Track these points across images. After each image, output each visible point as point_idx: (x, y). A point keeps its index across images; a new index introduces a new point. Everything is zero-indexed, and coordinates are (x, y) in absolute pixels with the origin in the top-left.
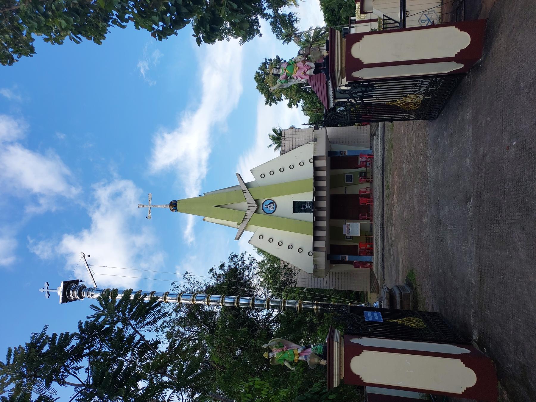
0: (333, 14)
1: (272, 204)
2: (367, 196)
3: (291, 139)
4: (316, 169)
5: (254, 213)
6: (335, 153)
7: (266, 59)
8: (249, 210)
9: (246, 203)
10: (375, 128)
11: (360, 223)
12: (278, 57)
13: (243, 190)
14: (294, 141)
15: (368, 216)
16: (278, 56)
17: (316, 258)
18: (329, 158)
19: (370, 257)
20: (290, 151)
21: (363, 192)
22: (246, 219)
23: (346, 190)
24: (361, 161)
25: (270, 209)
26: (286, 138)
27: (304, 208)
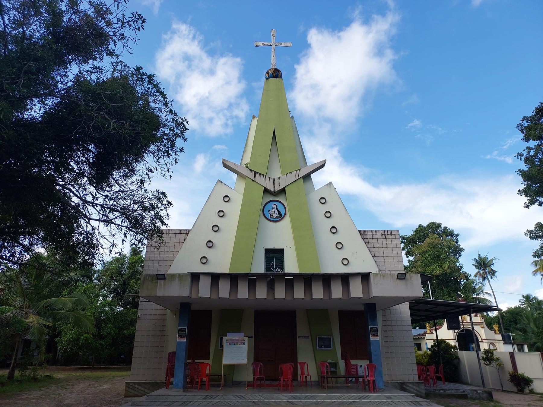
0: (511, 322)
1: (278, 216)
2: (295, 378)
3: (385, 245)
4: (345, 279)
5: (265, 187)
6: (374, 317)
7: (458, 235)
8: (269, 179)
9: (280, 175)
10: (416, 390)
11: (246, 365)
12: (462, 250)
13: (300, 170)
14: (381, 250)
15: (260, 379)
16: (464, 250)
17: (177, 279)
18: (361, 308)
19: (181, 385)
20: (365, 243)
21: (302, 369)
22: (255, 175)
23: (304, 337)
24: (356, 365)
25: (271, 212)
26: (385, 237)
27: (273, 267)
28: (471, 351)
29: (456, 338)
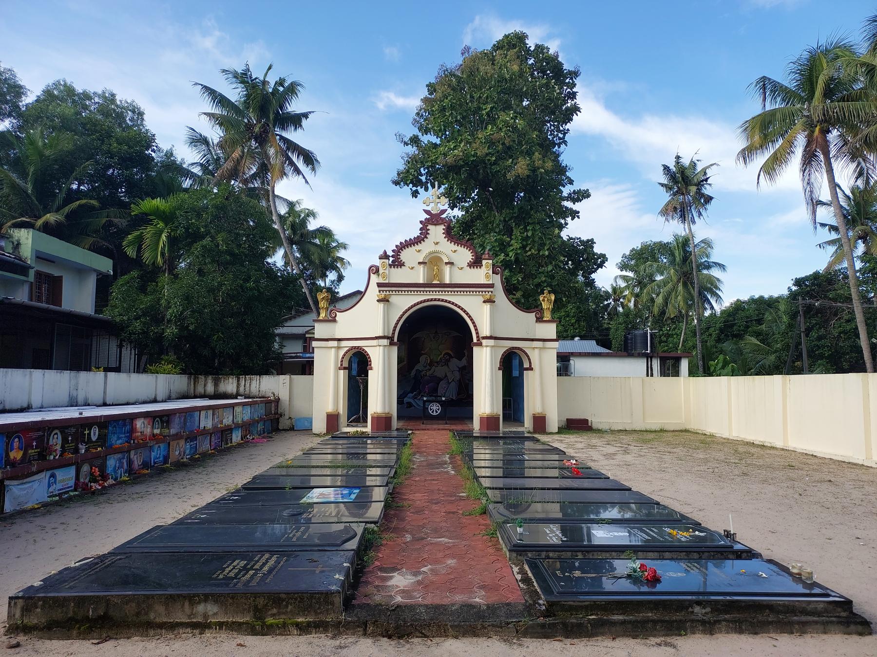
28: (869, 372)
29: (393, 334)
